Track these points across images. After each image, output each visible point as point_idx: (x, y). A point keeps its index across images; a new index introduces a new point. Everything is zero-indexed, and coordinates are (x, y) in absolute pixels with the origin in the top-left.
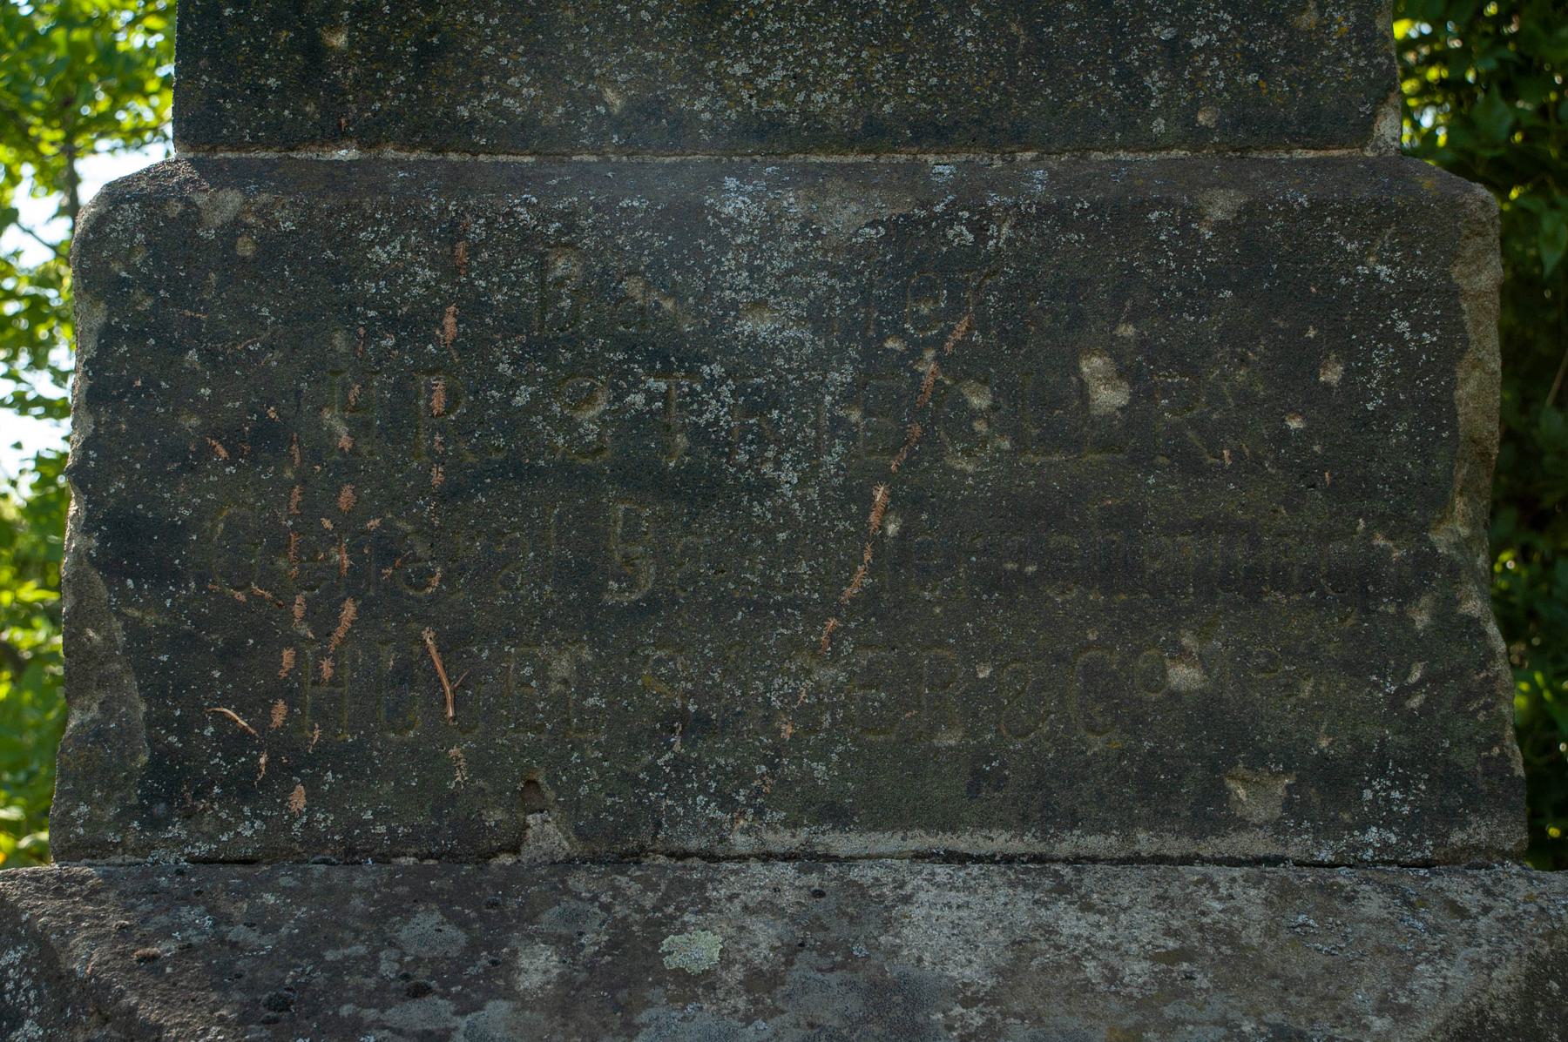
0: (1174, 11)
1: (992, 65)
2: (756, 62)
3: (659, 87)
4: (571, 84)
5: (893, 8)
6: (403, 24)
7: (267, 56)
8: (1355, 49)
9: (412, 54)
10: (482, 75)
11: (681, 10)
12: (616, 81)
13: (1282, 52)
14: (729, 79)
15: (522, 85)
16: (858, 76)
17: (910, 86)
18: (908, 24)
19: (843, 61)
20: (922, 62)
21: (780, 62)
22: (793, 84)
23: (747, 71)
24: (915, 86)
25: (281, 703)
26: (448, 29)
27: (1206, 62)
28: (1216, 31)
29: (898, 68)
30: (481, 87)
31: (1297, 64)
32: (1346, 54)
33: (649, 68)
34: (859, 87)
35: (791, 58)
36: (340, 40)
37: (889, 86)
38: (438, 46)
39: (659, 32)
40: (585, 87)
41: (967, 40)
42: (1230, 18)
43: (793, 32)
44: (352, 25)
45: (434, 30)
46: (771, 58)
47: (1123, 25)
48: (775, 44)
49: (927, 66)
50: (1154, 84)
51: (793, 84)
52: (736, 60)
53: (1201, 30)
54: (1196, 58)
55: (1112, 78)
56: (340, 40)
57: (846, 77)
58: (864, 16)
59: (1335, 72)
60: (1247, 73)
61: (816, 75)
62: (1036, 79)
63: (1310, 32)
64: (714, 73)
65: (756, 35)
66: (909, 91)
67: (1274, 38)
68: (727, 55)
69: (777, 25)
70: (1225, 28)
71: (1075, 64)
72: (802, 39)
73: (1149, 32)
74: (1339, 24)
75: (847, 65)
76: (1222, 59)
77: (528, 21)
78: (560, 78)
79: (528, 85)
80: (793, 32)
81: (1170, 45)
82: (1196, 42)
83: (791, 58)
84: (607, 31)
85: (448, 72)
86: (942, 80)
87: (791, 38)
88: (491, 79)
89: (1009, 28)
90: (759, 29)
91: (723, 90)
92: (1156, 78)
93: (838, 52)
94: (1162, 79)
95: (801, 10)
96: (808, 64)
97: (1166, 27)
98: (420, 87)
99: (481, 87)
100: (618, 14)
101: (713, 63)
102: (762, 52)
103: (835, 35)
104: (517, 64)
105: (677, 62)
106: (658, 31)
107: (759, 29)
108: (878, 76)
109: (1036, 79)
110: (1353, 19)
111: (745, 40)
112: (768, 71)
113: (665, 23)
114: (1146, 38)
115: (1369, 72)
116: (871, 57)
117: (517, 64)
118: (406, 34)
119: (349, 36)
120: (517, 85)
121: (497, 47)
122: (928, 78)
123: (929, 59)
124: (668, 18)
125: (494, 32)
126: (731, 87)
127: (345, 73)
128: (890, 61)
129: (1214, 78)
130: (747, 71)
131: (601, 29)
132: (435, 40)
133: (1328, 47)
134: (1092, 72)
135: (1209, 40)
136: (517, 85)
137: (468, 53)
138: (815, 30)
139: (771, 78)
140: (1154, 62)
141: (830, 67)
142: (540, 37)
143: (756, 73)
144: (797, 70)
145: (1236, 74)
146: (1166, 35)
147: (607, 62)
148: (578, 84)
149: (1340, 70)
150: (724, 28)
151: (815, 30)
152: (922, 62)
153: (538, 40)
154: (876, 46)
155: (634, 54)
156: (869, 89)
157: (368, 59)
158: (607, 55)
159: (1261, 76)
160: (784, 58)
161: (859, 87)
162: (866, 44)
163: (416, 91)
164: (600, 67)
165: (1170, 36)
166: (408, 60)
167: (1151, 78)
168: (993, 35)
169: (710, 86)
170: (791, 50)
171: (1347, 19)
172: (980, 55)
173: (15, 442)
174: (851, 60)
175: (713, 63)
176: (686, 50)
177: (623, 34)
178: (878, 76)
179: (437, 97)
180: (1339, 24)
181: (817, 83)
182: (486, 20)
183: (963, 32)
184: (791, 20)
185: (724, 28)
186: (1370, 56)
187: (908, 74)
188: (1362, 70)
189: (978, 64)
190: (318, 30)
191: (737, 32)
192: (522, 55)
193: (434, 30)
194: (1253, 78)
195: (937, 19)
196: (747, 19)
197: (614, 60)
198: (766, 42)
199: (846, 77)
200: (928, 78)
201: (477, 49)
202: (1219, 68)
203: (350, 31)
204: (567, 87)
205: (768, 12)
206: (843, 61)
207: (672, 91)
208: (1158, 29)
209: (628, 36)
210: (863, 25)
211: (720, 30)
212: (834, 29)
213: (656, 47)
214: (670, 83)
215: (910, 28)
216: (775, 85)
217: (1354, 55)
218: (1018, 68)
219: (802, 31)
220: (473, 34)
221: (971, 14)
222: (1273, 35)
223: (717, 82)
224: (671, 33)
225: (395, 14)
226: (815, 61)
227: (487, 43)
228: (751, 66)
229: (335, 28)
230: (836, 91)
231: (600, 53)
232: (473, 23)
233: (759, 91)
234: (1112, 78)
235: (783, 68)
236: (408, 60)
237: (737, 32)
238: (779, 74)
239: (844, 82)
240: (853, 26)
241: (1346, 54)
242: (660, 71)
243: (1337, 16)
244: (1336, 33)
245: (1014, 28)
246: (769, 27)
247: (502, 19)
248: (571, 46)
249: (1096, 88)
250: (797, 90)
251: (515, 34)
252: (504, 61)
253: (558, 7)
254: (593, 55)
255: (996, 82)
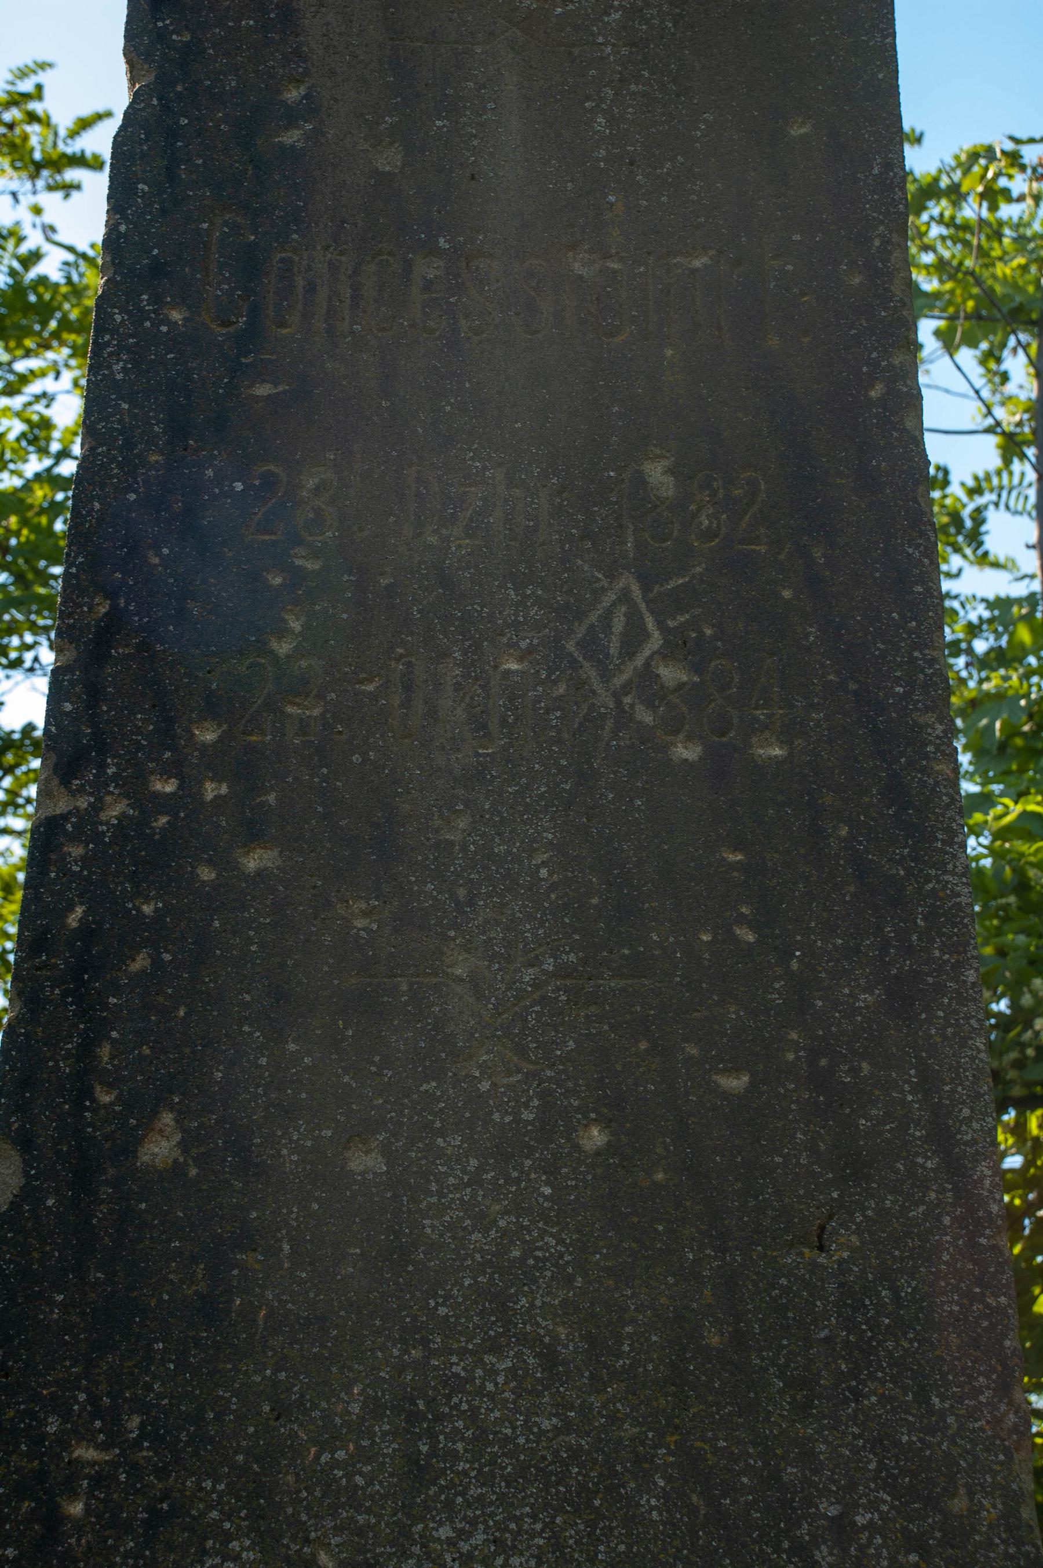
0: (838, 1489)
1: (675, 1534)
2: (459, 1526)
3: (369, 1551)
4: (288, 1547)
5: (584, 1476)
6: (137, 1492)
7: (8, 1527)
8: (1004, 1536)
9: (143, 1520)
10: (206, 1539)
11: (392, 1475)
12: (330, 1544)
13: (938, 1535)
14: (434, 1542)
15: (243, 1549)
16: (553, 1541)
17: (600, 1552)
18: (598, 1492)
19: (538, 1526)
20: (611, 1529)
21: (481, 1527)
22: (493, 1548)
23: (451, 1534)
24: (605, 1552)
25: (746, 1079)
26: (178, 1495)
27: (871, 1538)
28: (878, 1510)
29: (589, 1535)
30: (205, 1552)
31: (952, 1547)
32: (997, 1541)
33: (361, 1531)
34: (554, 1552)
35: (491, 1523)
36: (77, 1509)
37: (581, 1551)
38: (166, 1512)
39: (371, 1497)
40: (301, 1549)
41: (652, 1508)
42: (889, 1499)
43: (494, 1498)
44: (90, 1494)
45: (165, 1497)
46: (473, 1523)
47: (793, 1500)
48: (477, 1508)
49: (616, 1533)
50: (823, 1558)
51: (493, 1548)
52: (441, 1523)
53: (864, 1509)
54: (861, 1536)
55: (785, 1551)
56: (77, 1509)
57: (541, 1542)
58: (558, 1483)
59: (987, 1557)
60: (907, 1553)
61: (514, 1540)
62: (716, 1549)
63: (962, 1516)
64: (421, 1537)
65: (459, 1500)
66: (600, 1556)
67: (930, 1520)
68: (433, 1518)
69: (479, 1491)
70: (885, 1508)
71: (750, 1536)
72: (501, 1504)
73: (817, 1508)
74: (988, 1511)
75: (543, 1531)
76: (884, 1537)
77: (251, 1486)
78: (277, 1541)
79: (248, 1549)
80: (494, 1498)
81: (836, 1520)
82: (860, 1520)
83: (491, 1523)
84: (323, 1496)
85: (175, 1538)
86: (629, 1547)
87: (491, 1503)
88: (214, 1543)
89: (689, 1498)
90: (463, 1494)
91: (428, 1554)
92: (825, 1553)
93: (534, 1517)
94: (831, 1554)
95: (502, 1476)
96: (507, 1529)
97: (832, 1504)
98: (147, 1553)
99: (205, 1552)
100: (336, 1480)
101: (420, 1526)
102: (465, 1517)
103: (532, 1500)
104: (239, 1528)
105: (387, 1525)
106: (370, 1495)
107: (463, 1494)
108: (571, 1542)
109: (716, 1549)
110: (1000, 1506)
111: (449, 1504)
112: (470, 1535)
113: (377, 1487)
114: (815, 1513)
115: (1019, 1559)
116: (565, 1522)
117: (239, 1528)
118: (139, 1502)
119: (86, 1504)
120: (238, 1549)
121: (221, 1512)
122: (617, 1545)
123: (618, 1526)
124: (380, 1483)
125: (220, 1497)
126: (435, 1550)
127: (79, 1540)
128: (582, 1527)
129: (878, 1555)
130: (451, 1534)
131: (318, 1494)
132: (165, 1506)
133: (980, 1533)
134: (766, 1544)
135: (872, 1519)
136: (238, 1549)
137: (194, 1518)
138: (514, 1496)
139: (473, 1542)
140: (822, 1537)
141: (527, 1532)
142: (262, 1501)
143: (459, 1537)
144: (497, 1534)
145: (898, 1553)
146: (833, 1511)
147: (323, 1526)
148: (295, 1547)
149: (992, 1555)
150: (431, 1493)
151: (514, 1496)
152: (611, 1529)
153: (260, 1505)
154: (568, 1512)
155: (347, 1518)
156: (563, 1554)
157: (102, 1526)
158: (323, 1518)
159: (921, 1557)
160: (485, 1522)
161: (554, 1552)
162: (560, 1510)
163: (143, 1557)
164: (316, 1531)
165: (836, 1513)
166: (139, 1526)
167: (821, 1552)
168: (675, 1505)
169: (416, 1549)
170: (492, 1515)
171: (994, 1506)
172: (664, 1524)
173: (926, 141)
174: (546, 1525)
175: (420, 1526)
176: (395, 1514)
177: (338, 1498)
178: (571, 1542)
179: (163, 1562)
180: (988, 1511)
181: (514, 1547)
182: (214, 1486)
183: (648, 1501)
184: (492, 1486)
185: (431, 1493)
186: (1019, 1543)
187: (598, 1540)
188: (1012, 1558)
189: (662, 1533)
190: (58, 1499)
191: (443, 1497)
192: (244, 1519)
193: (165, 1497)
194: (913, 1558)
195: (625, 1488)
196: (452, 1485)
197: (329, 1523)
198: (469, 1506)
199: (541, 1542)
200: (617, 1545)
201: (203, 1514)
202: (882, 1546)
203: (87, 1499)
204: (284, 1550)
205: (471, 1478)
206: (538, 1526)
207: (381, 1554)
208: (825, 1505)
209: (343, 1500)
210: (558, 1492)
211: (427, 1494)
212: (531, 1496)
213: (369, 1511)
214: (380, 1546)
215: (600, 1495)
216: (476, 1548)
217: (1003, 1541)
218: (699, 1538)
219: (502, 1497)
220: (201, 1499)
221: (655, 1484)
222: (929, 1517)
223: (423, 1546)
224: (383, 1497)
225: (131, 1482)
226: (513, 1526)
227: (211, 1508)
228: (454, 1529)
229: (73, 1495)
230: (532, 1556)
231: (316, 1516)
232: (201, 1489)
233: (462, 1555)
234: (785, 1551)
235: (484, 1532)
236: (139, 1526)
237: (443, 1497)
238: (479, 1538)
239: (539, 1547)
240: (548, 1493)
241: (997, 1541)
242: (371, 1534)
243: (985, 1502)
244: (985, 1519)
245: (694, 1498)
246: (471, 1492)
247: (227, 1485)
248: (290, 1510)
249: (771, 1560)
250: (496, 1554)
251: (238, 1498)
252: (227, 1525)
253: (280, 1473)
254: (309, 1519)
255: (679, 1551)
